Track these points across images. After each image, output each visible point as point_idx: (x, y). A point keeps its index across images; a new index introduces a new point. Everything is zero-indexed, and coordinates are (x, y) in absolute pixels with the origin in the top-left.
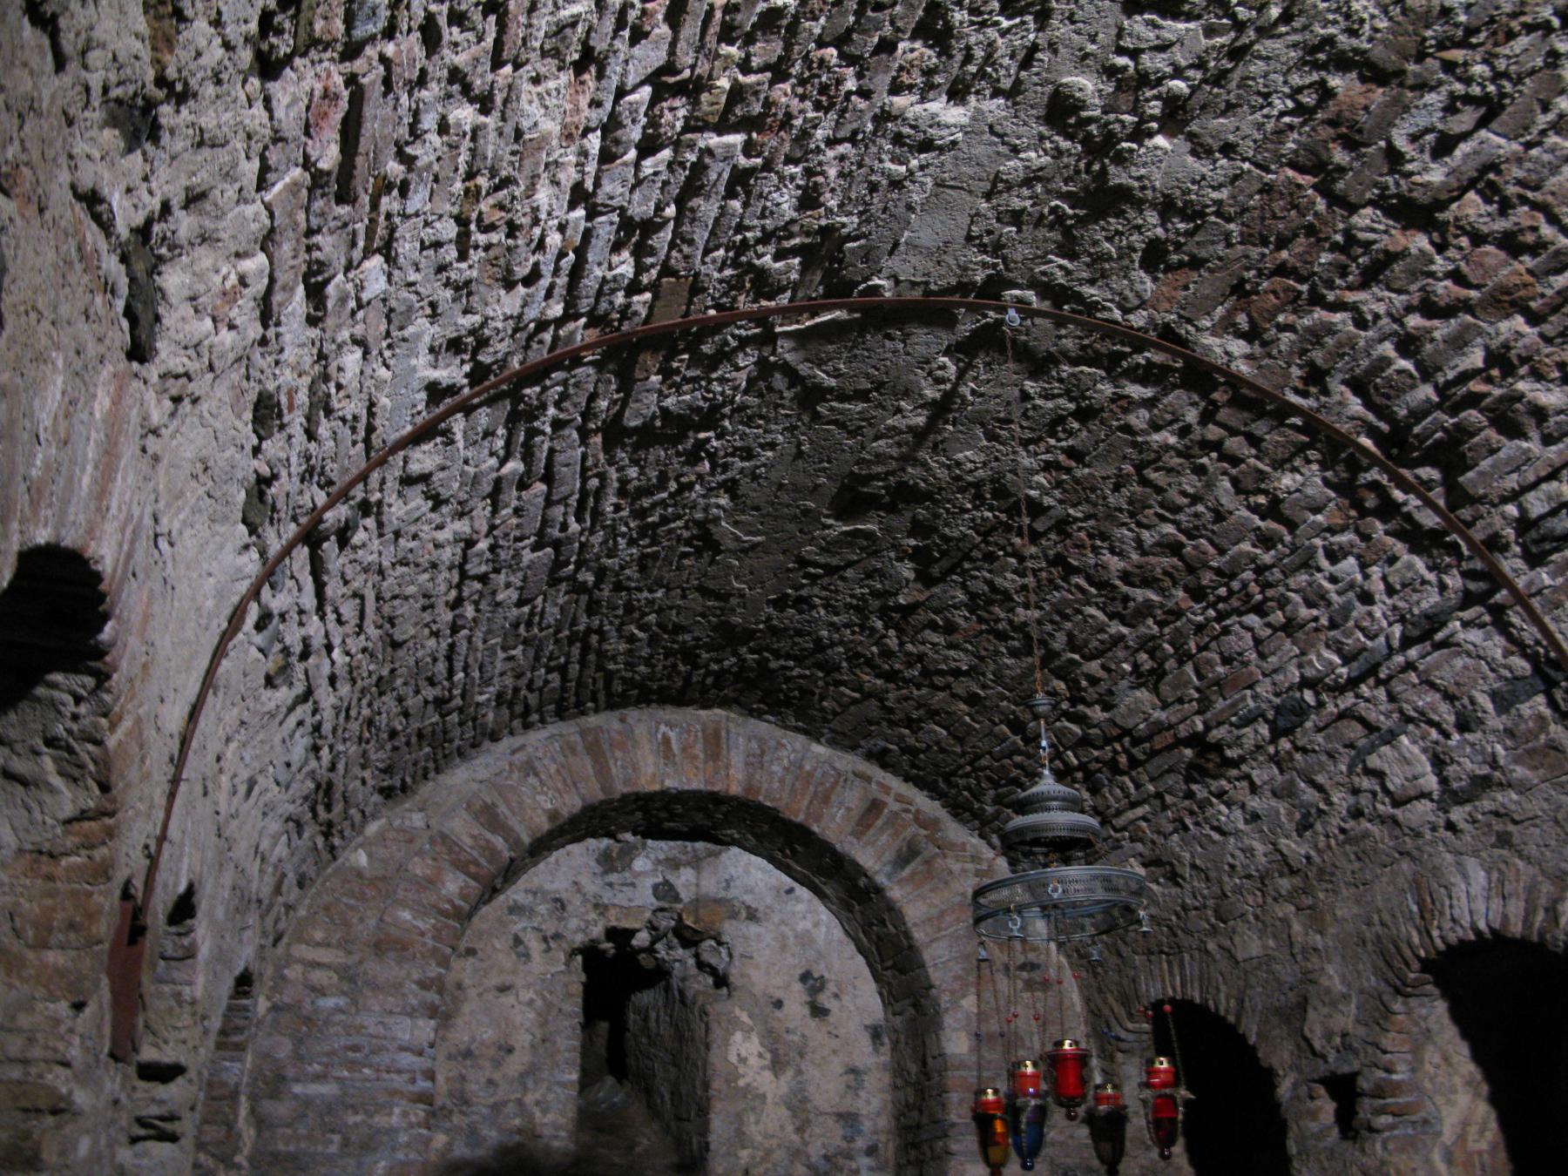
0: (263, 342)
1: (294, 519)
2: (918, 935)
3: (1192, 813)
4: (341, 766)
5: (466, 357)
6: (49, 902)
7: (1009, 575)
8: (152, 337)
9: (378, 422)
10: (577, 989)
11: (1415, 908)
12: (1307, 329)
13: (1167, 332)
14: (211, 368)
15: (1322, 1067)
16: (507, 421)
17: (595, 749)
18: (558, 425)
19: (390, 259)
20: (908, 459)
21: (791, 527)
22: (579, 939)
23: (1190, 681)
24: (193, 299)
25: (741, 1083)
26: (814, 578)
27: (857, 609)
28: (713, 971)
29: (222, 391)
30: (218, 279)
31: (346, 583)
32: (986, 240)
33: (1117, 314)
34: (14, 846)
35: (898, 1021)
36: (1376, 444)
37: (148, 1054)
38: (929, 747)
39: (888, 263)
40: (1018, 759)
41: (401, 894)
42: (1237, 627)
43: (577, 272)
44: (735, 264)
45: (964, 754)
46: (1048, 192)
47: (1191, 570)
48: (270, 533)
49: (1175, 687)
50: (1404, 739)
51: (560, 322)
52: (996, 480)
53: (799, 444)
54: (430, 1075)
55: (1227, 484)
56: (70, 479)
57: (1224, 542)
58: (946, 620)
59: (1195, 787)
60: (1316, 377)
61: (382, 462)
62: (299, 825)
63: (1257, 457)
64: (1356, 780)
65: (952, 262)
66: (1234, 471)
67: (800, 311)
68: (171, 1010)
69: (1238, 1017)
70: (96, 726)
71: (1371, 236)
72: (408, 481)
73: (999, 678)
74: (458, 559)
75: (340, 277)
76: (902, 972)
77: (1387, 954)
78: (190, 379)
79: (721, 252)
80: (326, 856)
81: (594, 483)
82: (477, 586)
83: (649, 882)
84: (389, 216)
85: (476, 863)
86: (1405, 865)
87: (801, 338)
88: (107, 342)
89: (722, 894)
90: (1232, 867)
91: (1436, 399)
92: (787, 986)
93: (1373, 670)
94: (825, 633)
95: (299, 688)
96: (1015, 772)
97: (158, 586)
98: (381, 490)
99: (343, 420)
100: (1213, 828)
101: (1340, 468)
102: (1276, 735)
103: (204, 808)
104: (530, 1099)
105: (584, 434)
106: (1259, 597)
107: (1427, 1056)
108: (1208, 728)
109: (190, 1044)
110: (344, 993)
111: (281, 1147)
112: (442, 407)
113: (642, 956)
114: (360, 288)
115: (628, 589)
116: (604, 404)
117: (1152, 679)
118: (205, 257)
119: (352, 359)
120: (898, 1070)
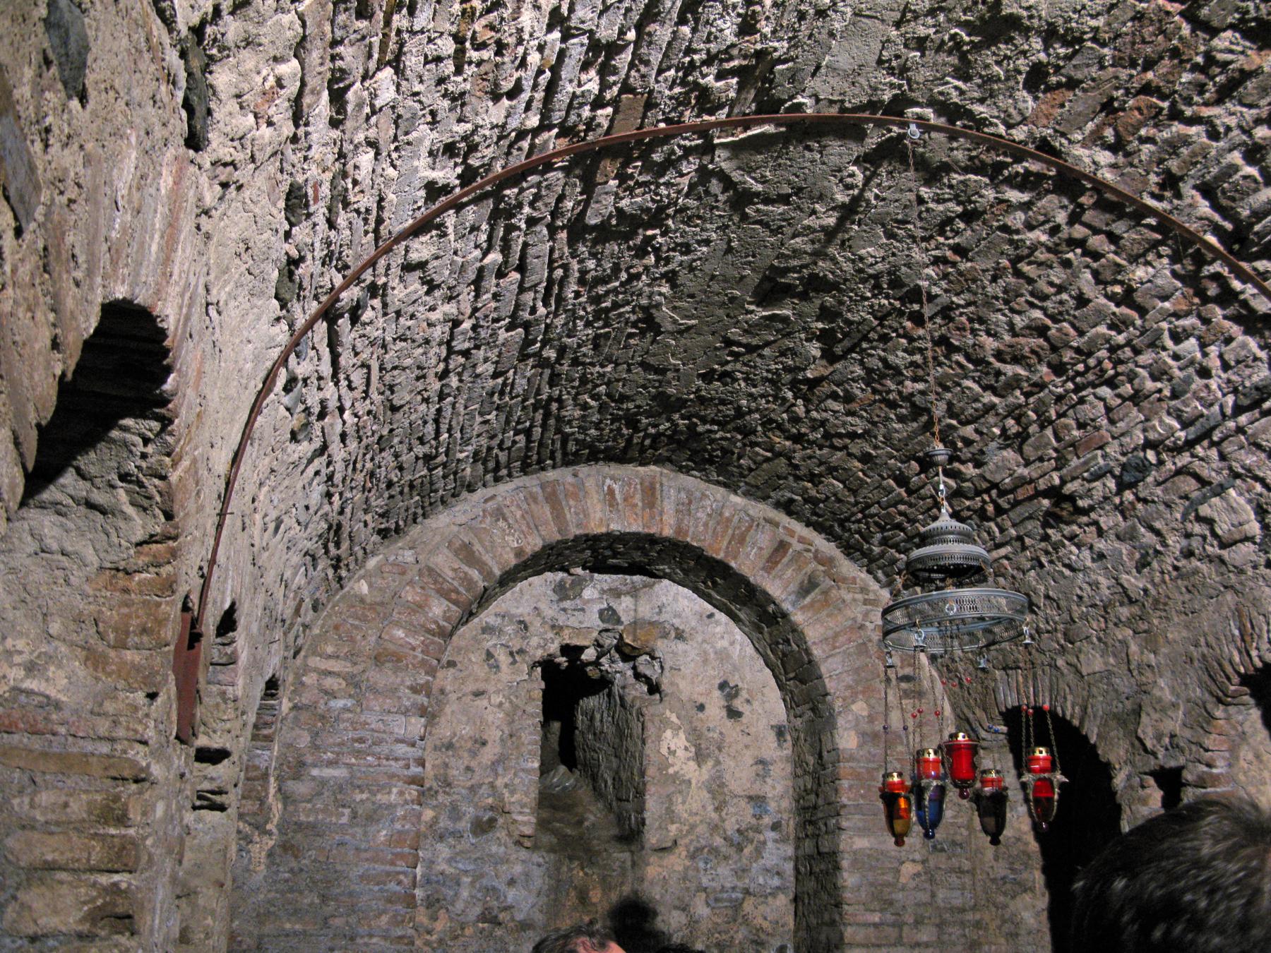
0: (294, 139)
1: (316, 297)
2: (817, 652)
3: (1047, 553)
4: (348, 510)
5: (459, 160)
6: (125, 610)
7: (900, 354)
8: (205, 128)
9: (386, 215)
10: (538, 694)
11: (1236, 632)
12: (1165, 141)
13: (1044, 145)
14: (253, 158)
15: (1152, 761)
16: (490, 218)
17: (552, 498)
18: (531, 222)
19: (399, 71)
20: (819, 254)
21: (721, 312)
22: (539, 654)
23: (1049, 443)
24: (238, 96)
25: (671, 771)
26: (736, 356)
27: (770, 381)
28: (648, 680)
29: (261, 181)
30: (259, 79)
31: (356, 354)
32: (894, 64)
33: (1002, 129)
34: (96, 565)
35: (798, 722)
36: (1221, 241)
37: (202, 741)
38: (828, 498)
39: (810, 83)
40: (902, 507)
41: (396, 616)
42: (1091, 398)
43: (552, 88)
44: (683, 83)
45: (857, 503)
46: (949, 20)
47: (1054, 349)
48: (296, 307)
49: (1036, 448)
50: (1232, 492)
51: (536, 132)
52: (893, 272)
53: (730, 241)
54: (421, 763)
55: (1088, 275)
56: (142, 244)
57: (1084, 326)
58: (846, 391)
59: (1050, 531)
60: (1171, 182)
61: (388, 250)
62: (314, 558)
63: (1116, 253)
64: (1189, 526)
65: (865, 83)
66: (1095, 265)
67: (736, 124)
68: (218, 705)
69: (1082, 721)
70: (160, 463)
71: (1229, 57)
72: (408, 268)
73: (888, 439)
74: (446, 337)
75: (358, 85)
76: (803, 682)
77: (1212, 671)
78: (236, 169)
79: (672, 72)
80: (335, 585)
81: (559, 273)
82: (461, 360)
83: (596, 607)
84: (399, 32)
85: (458, 593)
86: (1229, 597)
87: (735, 148)
88: (170, 127)
89: (656, 618)
90: (1080, 598)
91: (304, 679)
92: (709, 693)
93: (1207, 434)
94: (744, 402)
95: (317, 443)
96: (899, 519)
97: (209, 347)
98: (387, 275)
99: (358, 211)
100: (1065, 565)
101: (1187, 262)
102: (1122, 487)
103: (243, 539)
104: (500, 782)
105: (553, 230)
106: (1111, 372)
107: (1242, 754)
108: (1063, 482)
109: (234, 733)
110: (350, 696)
111: (303, 818)
112: (438, 204)
113: (589, 669)
114: (374, 95)
115: (583, 364)
116: (569, 204)
117: (1017, 441)
118: (248, 59)
119: (366, 159)
120: (798, 762)
